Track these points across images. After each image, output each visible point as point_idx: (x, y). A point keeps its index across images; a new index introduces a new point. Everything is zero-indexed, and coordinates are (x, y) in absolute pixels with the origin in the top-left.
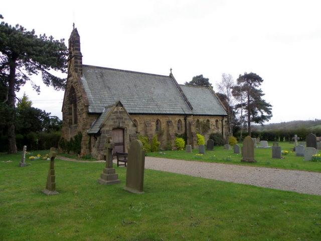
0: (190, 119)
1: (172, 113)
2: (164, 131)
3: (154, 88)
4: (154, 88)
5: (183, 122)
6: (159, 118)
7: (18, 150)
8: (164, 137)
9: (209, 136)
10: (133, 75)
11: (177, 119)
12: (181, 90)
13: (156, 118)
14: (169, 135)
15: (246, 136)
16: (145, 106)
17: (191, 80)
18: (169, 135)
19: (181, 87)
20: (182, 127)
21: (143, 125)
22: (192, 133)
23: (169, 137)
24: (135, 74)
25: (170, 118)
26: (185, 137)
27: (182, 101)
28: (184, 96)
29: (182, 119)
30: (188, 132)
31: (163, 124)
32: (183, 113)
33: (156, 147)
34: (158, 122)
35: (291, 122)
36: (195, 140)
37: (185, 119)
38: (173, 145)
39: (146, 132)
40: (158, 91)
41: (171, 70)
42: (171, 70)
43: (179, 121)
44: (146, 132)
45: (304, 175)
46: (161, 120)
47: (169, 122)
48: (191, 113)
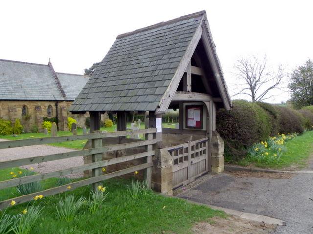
0: (60, 105)
1: (41, 99)
2: (31, 116)
3: (26, 76)
4: (26, 76)
5: (54, 108)
6: (26, 104)
7: (174, 155)
8: (32, 121)
9: (85, 119)
10: (4, 63)
11: (47, 104)
12: (57, 79)
13: (22, 104)
14: (36, 119)
15: (130, 121)
16: (10, 93)
17: (91, 66)
18: (36, 119)
19: (57, 75)
20: (52, 112)
21: (7, 111)
22: (62, 117)
23: (37, 121)
24: (6, 63)
25: (39, 104)
26: (56, 120)
27: (56, 89)
28: (59, 83)
29: (53, 104)
30: (59, 116)
31: (31, 110)
32: (54, 99)
33: (18, 130)
34: (24, 108)
35: (269, 104)
36: (66, 123)
37: (56, 105)
38: (39, 128)
39: (10, 117)
40: (31, 79)
41: (50, 59)
42: (50, 59)
43: (50, 107)
44: (10, 117)
45: (179, 147)
46: (28, 106)
47: (37, 108)
48: (63, 99)
